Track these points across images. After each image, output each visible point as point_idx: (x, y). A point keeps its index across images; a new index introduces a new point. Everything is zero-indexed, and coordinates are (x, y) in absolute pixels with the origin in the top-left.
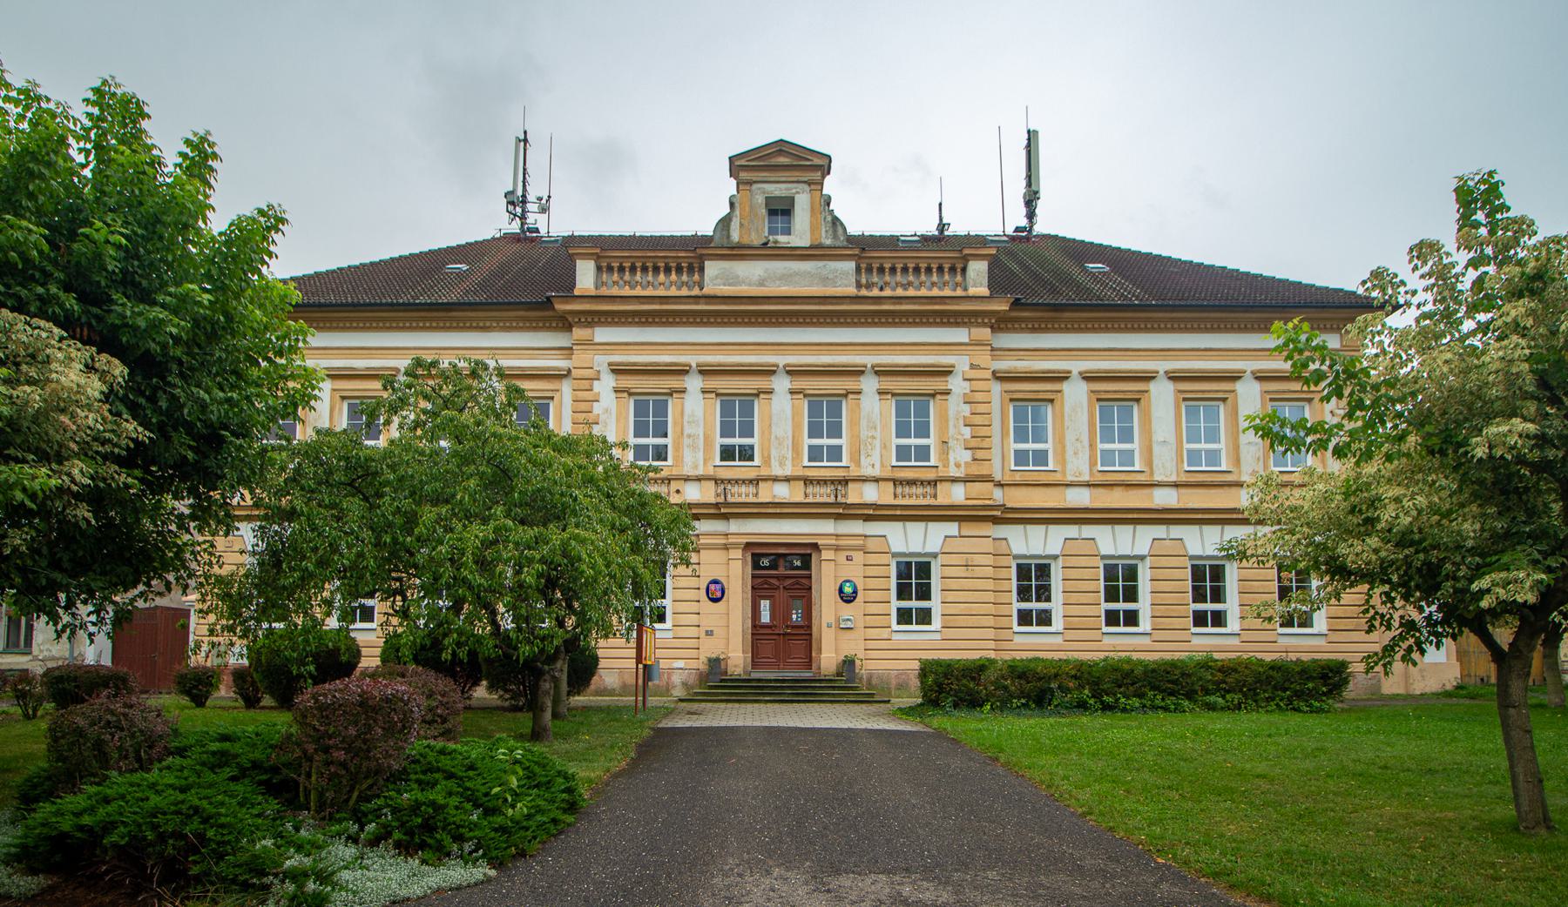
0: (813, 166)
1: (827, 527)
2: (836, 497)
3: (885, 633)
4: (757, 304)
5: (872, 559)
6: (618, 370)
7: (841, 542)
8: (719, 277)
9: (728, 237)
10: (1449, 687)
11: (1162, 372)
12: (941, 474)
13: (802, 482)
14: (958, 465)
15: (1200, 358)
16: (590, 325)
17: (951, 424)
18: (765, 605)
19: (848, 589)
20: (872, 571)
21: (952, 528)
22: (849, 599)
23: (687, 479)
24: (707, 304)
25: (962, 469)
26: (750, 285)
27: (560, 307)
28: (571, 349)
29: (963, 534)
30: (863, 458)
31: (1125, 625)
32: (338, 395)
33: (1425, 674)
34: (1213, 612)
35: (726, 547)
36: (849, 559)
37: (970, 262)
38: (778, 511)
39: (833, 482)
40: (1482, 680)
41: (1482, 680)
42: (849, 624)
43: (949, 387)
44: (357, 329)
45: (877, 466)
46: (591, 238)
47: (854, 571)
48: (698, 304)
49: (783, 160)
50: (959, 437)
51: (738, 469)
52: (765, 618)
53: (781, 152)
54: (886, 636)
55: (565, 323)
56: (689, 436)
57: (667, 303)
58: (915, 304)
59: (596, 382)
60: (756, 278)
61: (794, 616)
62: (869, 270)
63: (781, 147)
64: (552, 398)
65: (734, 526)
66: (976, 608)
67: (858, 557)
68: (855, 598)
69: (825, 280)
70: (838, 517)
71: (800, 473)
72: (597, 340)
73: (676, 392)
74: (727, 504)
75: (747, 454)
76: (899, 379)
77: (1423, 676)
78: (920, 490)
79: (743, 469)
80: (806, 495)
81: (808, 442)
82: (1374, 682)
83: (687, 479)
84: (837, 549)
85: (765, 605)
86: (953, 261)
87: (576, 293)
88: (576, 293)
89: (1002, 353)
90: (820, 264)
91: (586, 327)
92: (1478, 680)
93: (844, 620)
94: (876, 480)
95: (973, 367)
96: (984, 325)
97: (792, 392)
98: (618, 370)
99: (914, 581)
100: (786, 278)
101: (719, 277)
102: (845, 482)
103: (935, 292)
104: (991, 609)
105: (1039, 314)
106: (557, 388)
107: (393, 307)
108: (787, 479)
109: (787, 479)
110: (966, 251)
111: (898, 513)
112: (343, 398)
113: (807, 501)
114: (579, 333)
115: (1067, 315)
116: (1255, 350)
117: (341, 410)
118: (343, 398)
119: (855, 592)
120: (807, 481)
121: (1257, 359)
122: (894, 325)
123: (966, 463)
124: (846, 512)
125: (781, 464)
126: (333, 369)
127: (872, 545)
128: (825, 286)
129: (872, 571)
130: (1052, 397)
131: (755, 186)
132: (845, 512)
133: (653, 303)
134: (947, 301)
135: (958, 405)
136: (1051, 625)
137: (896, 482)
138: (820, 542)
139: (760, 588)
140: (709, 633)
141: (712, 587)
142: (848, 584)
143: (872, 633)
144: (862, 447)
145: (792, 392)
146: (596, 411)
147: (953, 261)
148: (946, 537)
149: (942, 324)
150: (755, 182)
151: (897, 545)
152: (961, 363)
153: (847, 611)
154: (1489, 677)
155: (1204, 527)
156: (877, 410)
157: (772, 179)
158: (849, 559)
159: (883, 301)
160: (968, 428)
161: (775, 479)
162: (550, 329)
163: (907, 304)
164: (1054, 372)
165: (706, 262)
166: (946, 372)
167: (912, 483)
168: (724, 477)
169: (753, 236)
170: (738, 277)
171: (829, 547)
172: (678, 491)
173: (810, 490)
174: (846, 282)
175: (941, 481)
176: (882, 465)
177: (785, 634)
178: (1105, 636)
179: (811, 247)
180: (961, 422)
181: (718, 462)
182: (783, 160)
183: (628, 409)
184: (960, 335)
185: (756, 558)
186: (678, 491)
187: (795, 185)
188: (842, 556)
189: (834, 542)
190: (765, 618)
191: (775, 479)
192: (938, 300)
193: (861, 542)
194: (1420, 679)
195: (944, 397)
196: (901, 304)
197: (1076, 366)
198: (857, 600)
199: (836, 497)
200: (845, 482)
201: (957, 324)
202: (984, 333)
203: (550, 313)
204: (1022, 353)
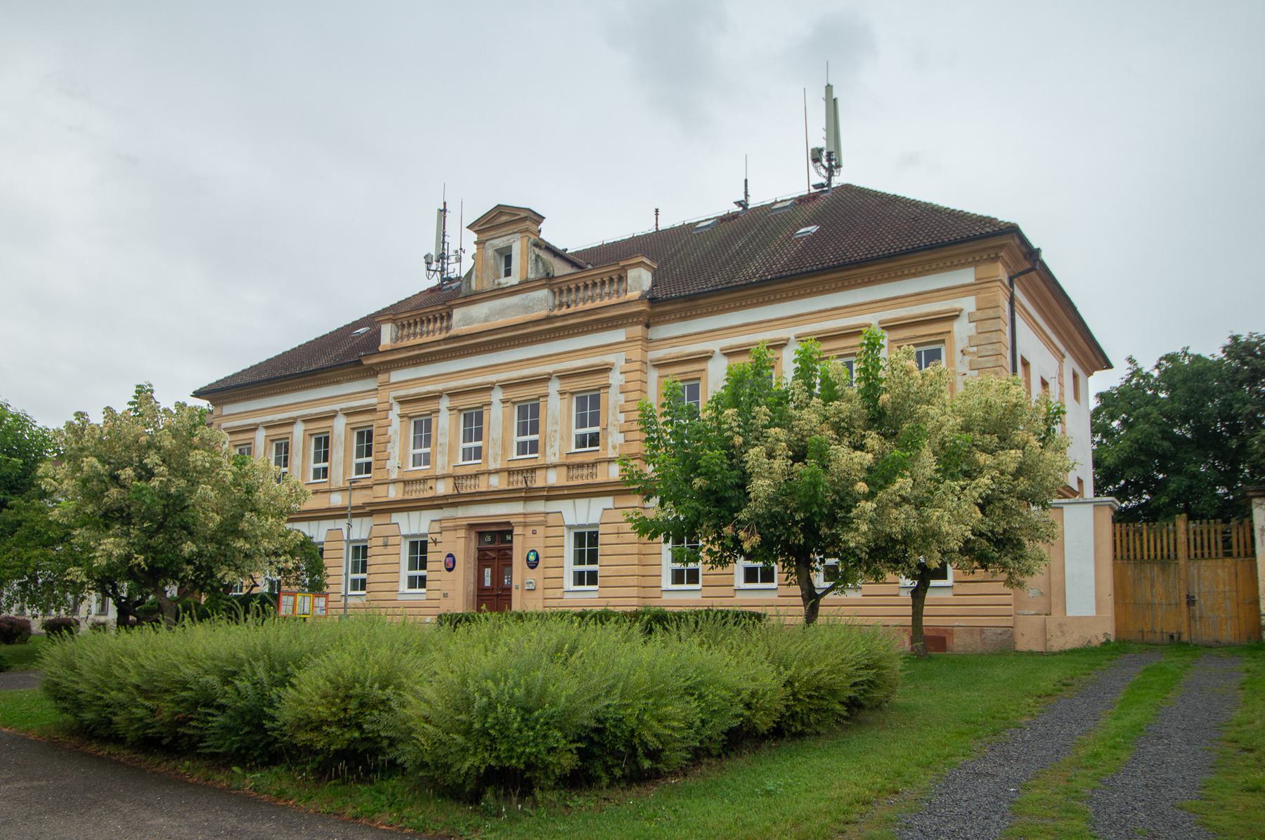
0: (527, 220)
1: (517, 508)
2: (526, 483)
3: (558, 593)
4: (476, 338)
5: (552, 532)
6: (403, 402)
7: (529, 520)
8: (468, 319)
9: (470, 287)
10: (1095, 643)
11: (792, 338)
12: (600, 457)
13: (506, 474)
14: (614, 447)
15: (828, 318)
16: (387, 370)
17: (610, 413)
18: (488, 571)
19: (532, 558)
20: (551, 542)
21: (608, 502)
22: (533, 565)
23: (437, 478)
24: (446, 344)
25: (617, 450)
26: (479, 322)
27: (367, 362)
28: (377, 390)
29: (616, 506)
30: (548, 448)
31: (762, 581)
32: (349, 427)
33: (1065, 628)
34: (420, 577)
35: (455, 528)
36: (534, 532)
37: (455, 311)
38: (483, 498)
39: (522, 471)
40: (1172, 637)
41: (1172, 637)
42: (531, 587)
43: (610, 382)
44: (915, 275)
45: (558, 455)
46: (385, 310)
47: (537, 543)
48: (440, 345)
49: (504, 219)
50: (616, 423)
51: (588, 454)
52: (488, 583)
53: (501, 213)
54: (559, 596)
55: (372, 372)
56: (441, 445)
57: (422, 349)
58: (576, 318)
59: (390, 412)
60: (483, 317)
61: (506, 581)
62: (561, 292)
63: (500, 210)
64: (943, 341)
65: (461, 512)
66: (623, 570)
67: (540, 530)
68: (537, 564)
69: (527, 308)
70: (526, 499)
71: (505, 466)
72: (392, 381)
73: (485, 405)
74: (459, 495)
75: (534, 446)
76: (570, 381)
77: (1062, 632)
78: (585, 472)
79: (471, 466)
80: (509, 483)
81: (517, 439)
82: (1005, 637)
83: (437, 478)
84: (525, 525)
85: (488, 571)
86: (618, 272)
87: (381, 349)
88: (381, 349)
89: (658, 343)
90: (524, 296)
91: (385, 372)
92: (1166, 637)
93: (527, 583)
94: (555, 466)
95: (627, 361)
96: (636, 324)
97: (504, 402)
98: (403, 402)
99: (586, 548)
100: (502, 312)
101: (468, 319)
102: (533, 470)
103: (589, 305)
104: (637, 570)
105: (679, 306)
106: (702, 368)
107: (286, 378)
108: (497, 472)
109: (497, 472)
110: (622, 264)
111: (566, 492)
112: (272, 441)
113: (511, 487)
114: (382, 378)
115: (701, 302)
116: (881, 301)
117: (271, 449)
118: (272, 441)
119: (537, 559)
120: (510, 472)
121: (885, 308)
122: (532, 343)
123: (620, 444)
124: (528, 495)
125: (495, 460)
126: (306, 416)
127: (551, 520)
128: (527, 313)
129: (551, 542)
130: (698, 376)
131: (488, 243)
132: (529, 495)
133: (414, 350)
134: (599, 311)
135: (616, 395)
136: (946, 579)
137: (569, 467)
138: (512, 521)
139: (483, 559)
140: (445, 595)
141: (448, 559)
142: (532, 554)
143: (550, 593)
144: (547, 440)
145: (504, 402)
146: (390, 433)
147: (618, 272)
148: (604, 509)
149: (519, 345)
150: (487, 240)
151: (570, 519)
152: (968, 304)
153: (532, 575)
154: (1180, 634)
155: (411, 513)
156: (558, 407)
157: (497, 235)
158: (534, 532)
159: (554, 320)
160: (623, 414)
161: (490, 473)
162: (364, 378)
163: (571, 319)
164: (695, 354)
165: (382, 326)
166: (606, 369)
167: (580, 466)
168: (588, 462)
169: (485, 283)
170: (472, 317)
171: (519, 524)
172: (431, 488)
173: (409, 488)
174: (540, 307)
175: (600, 462)
176: (560, 454)
177: (498, 595)
178: (737, 592)
179: (520, 283)
180: (618, 411)
181: (411, 468)
182: (504, 219)
183: (352, 440)
184: (618, 335)
185: (481, 535)
186: (431, 488)
187: (513, 236)
188: (529, 530)
189: (522, 520)
190: (488, 583)
191: (490, 473)
192: (592, 312)
193: (543, 518)
194: (1059, 634)
195: (606, 390)
196: (567, 320)
197: (715, 345)
198: (539, 566)
199: (526, 483)
200: (533, 470)
201: (616, 327)
202: (638, 330)
203: (361, 368)
204: (674, 340)
